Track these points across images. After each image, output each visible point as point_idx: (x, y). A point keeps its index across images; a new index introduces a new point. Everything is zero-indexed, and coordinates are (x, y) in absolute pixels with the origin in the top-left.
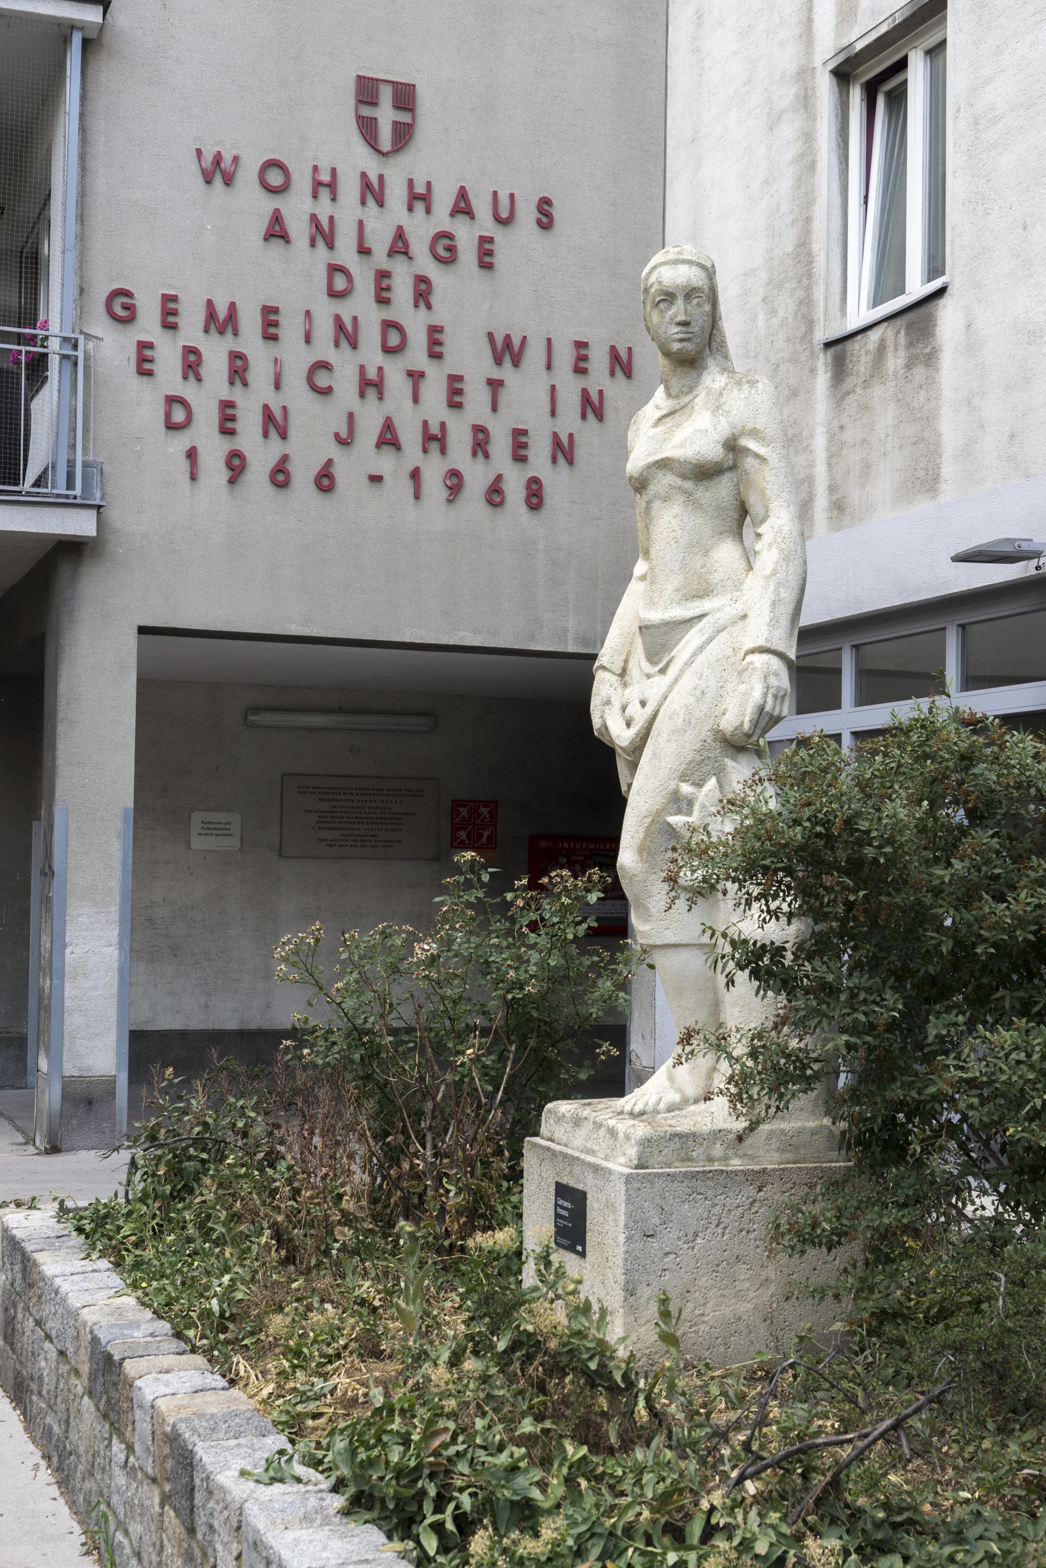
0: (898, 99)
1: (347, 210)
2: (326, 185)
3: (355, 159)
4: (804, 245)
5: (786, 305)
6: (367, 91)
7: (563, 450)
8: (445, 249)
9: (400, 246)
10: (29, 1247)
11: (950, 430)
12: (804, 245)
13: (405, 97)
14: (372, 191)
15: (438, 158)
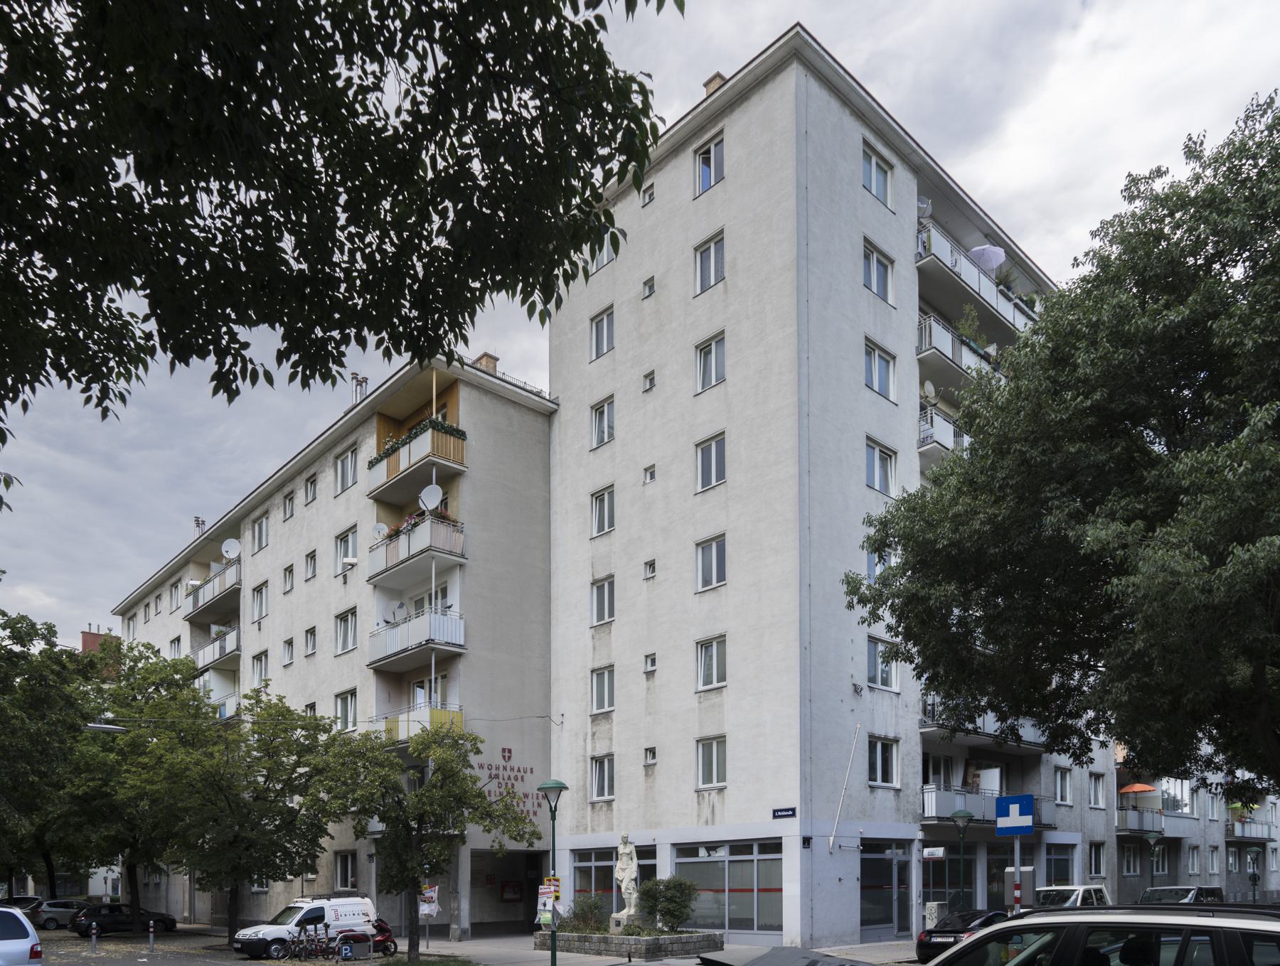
0: (347, 542)
1: (501, 772)
2: (498, 768)
3: (502, 763)
4: (585, 785)
5: (581, 794)
6: (504, 750)
7: (535, 813)
8: (516, 779)
9: (509, 778)
10: (393, 458)
11: (615, 821)
12: (585, 785)
13: (510, 751)
14: (505, 768)
15: (515, 762)
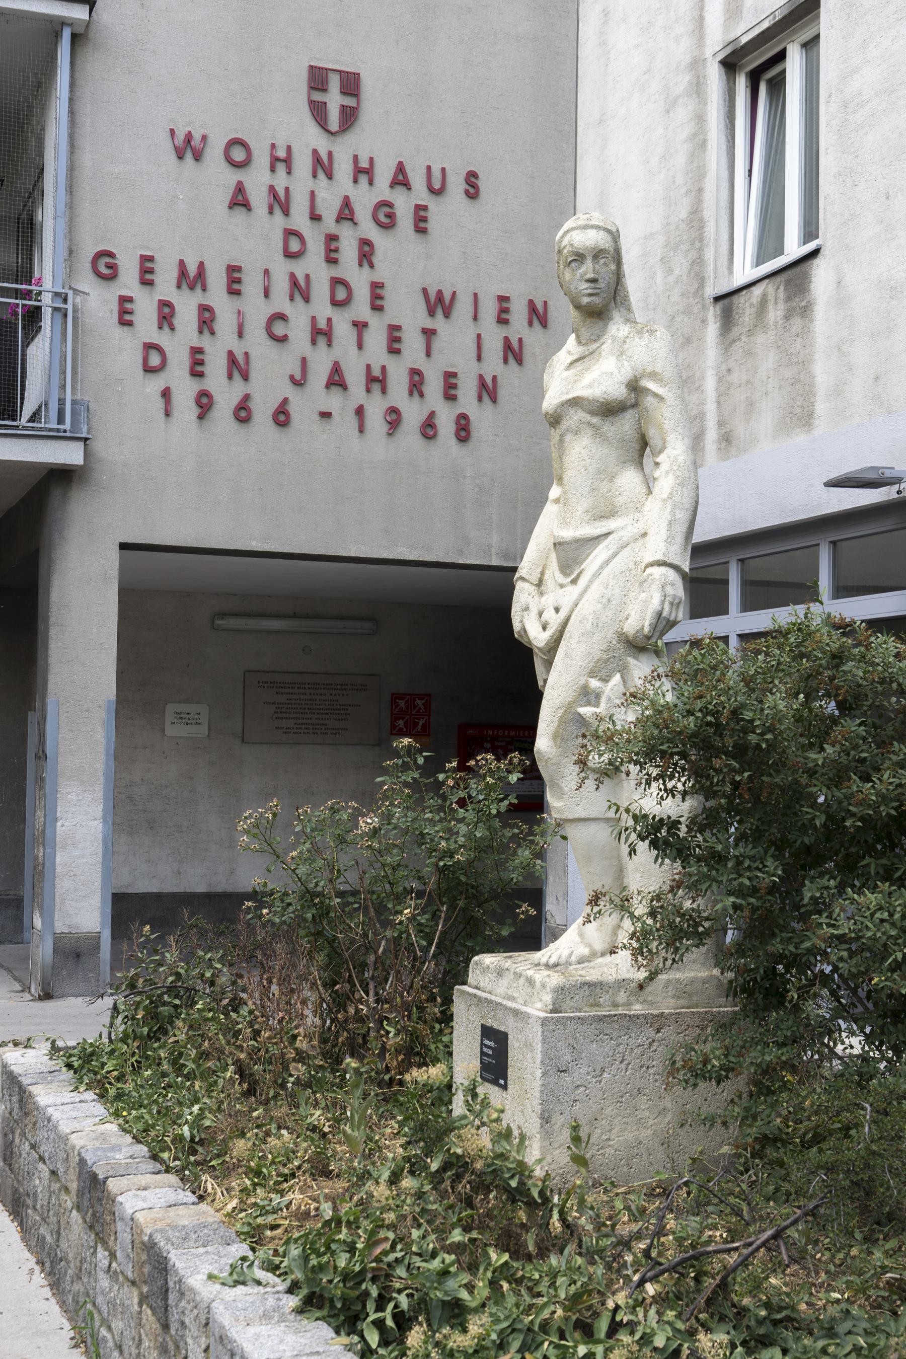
0: (778, 86)
1: (301, 182)
2: (282, 161)
3: (307, 138)
4: (696, 212)
5: (681, 264)
6: (318, 78)
7: (488, 390)
8: (385, 216)
9: (346, 213)
10: (25, 1081)
11: (823, 373)
12: (696, 212)
13: (351, 84)
14: (323, 166)
15: (379, 137)
